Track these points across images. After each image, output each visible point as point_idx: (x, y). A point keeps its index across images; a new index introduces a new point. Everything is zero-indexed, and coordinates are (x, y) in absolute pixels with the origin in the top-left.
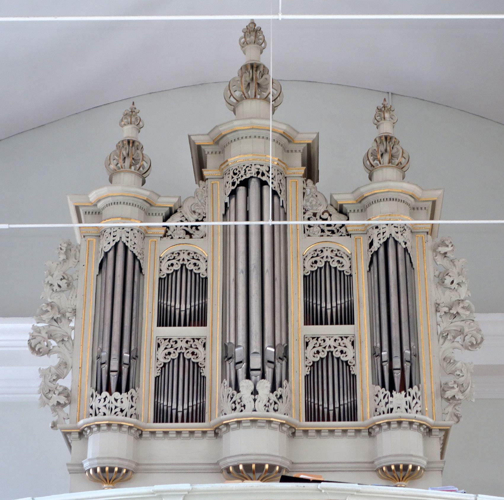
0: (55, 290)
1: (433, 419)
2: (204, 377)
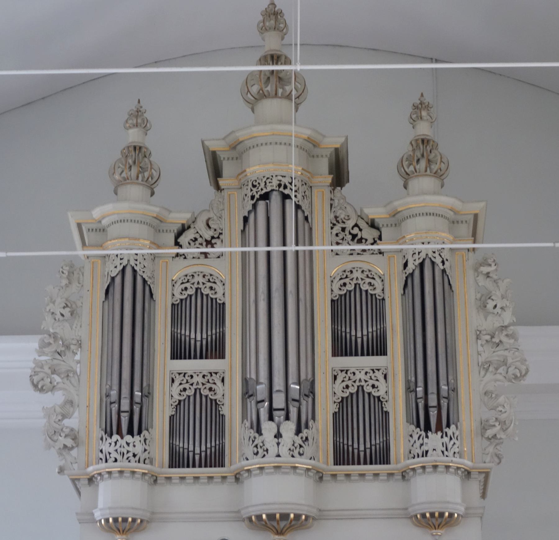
0: (57, 319)
1: (472, 461)
2: (223, 415)
